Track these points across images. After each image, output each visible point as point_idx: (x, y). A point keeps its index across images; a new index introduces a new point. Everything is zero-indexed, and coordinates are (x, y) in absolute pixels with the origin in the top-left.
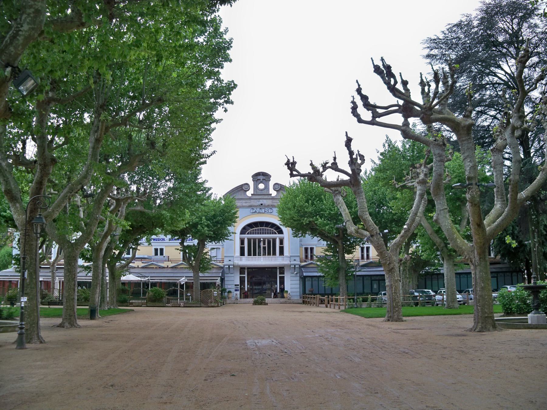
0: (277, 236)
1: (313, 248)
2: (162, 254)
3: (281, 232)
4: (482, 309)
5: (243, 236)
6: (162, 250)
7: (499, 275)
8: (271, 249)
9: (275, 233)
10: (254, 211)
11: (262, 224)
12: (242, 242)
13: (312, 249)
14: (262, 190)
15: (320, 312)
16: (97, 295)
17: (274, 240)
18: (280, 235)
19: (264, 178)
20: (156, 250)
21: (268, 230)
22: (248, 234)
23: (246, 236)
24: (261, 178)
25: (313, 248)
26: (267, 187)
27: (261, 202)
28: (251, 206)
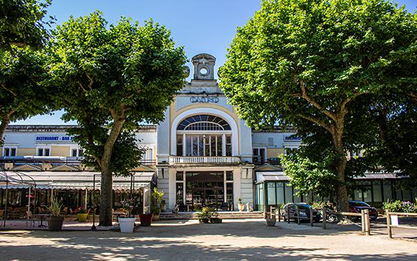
0: (224, 133)
1: (15, 149)
2: (13, 154)
3: (228, 128)
4: (136, 196)
5: (181, 132)
6: (14, 150)
7: (374, 183)
8: (215, 148)
9: (221, 129)
10: (195, 100)
11: (204, 117)
12: (179, 141)
13: (262, 151)
14: (204, 75)
15: (304, 250)
16: (76, 247)
17: (220, 138)
18: (228, 132)
19: (207, 61)
20: (7, 150)
21: (212, 124)
22: (187, 129)
23: (184, 132)
24: (203, 61)
25: (15, 149)
26: (211, 72)
27: (203, 89)
28: (191, 93)
